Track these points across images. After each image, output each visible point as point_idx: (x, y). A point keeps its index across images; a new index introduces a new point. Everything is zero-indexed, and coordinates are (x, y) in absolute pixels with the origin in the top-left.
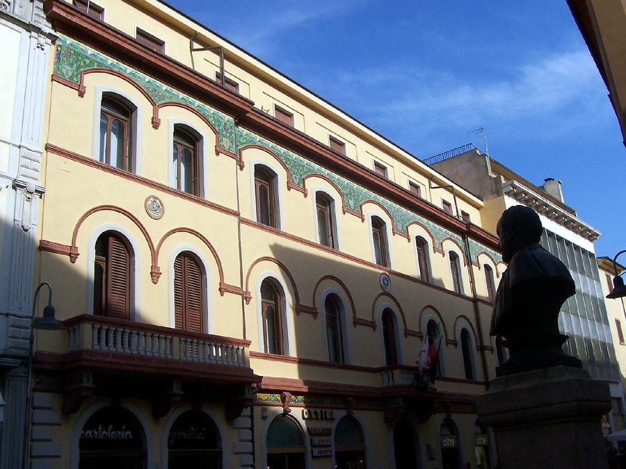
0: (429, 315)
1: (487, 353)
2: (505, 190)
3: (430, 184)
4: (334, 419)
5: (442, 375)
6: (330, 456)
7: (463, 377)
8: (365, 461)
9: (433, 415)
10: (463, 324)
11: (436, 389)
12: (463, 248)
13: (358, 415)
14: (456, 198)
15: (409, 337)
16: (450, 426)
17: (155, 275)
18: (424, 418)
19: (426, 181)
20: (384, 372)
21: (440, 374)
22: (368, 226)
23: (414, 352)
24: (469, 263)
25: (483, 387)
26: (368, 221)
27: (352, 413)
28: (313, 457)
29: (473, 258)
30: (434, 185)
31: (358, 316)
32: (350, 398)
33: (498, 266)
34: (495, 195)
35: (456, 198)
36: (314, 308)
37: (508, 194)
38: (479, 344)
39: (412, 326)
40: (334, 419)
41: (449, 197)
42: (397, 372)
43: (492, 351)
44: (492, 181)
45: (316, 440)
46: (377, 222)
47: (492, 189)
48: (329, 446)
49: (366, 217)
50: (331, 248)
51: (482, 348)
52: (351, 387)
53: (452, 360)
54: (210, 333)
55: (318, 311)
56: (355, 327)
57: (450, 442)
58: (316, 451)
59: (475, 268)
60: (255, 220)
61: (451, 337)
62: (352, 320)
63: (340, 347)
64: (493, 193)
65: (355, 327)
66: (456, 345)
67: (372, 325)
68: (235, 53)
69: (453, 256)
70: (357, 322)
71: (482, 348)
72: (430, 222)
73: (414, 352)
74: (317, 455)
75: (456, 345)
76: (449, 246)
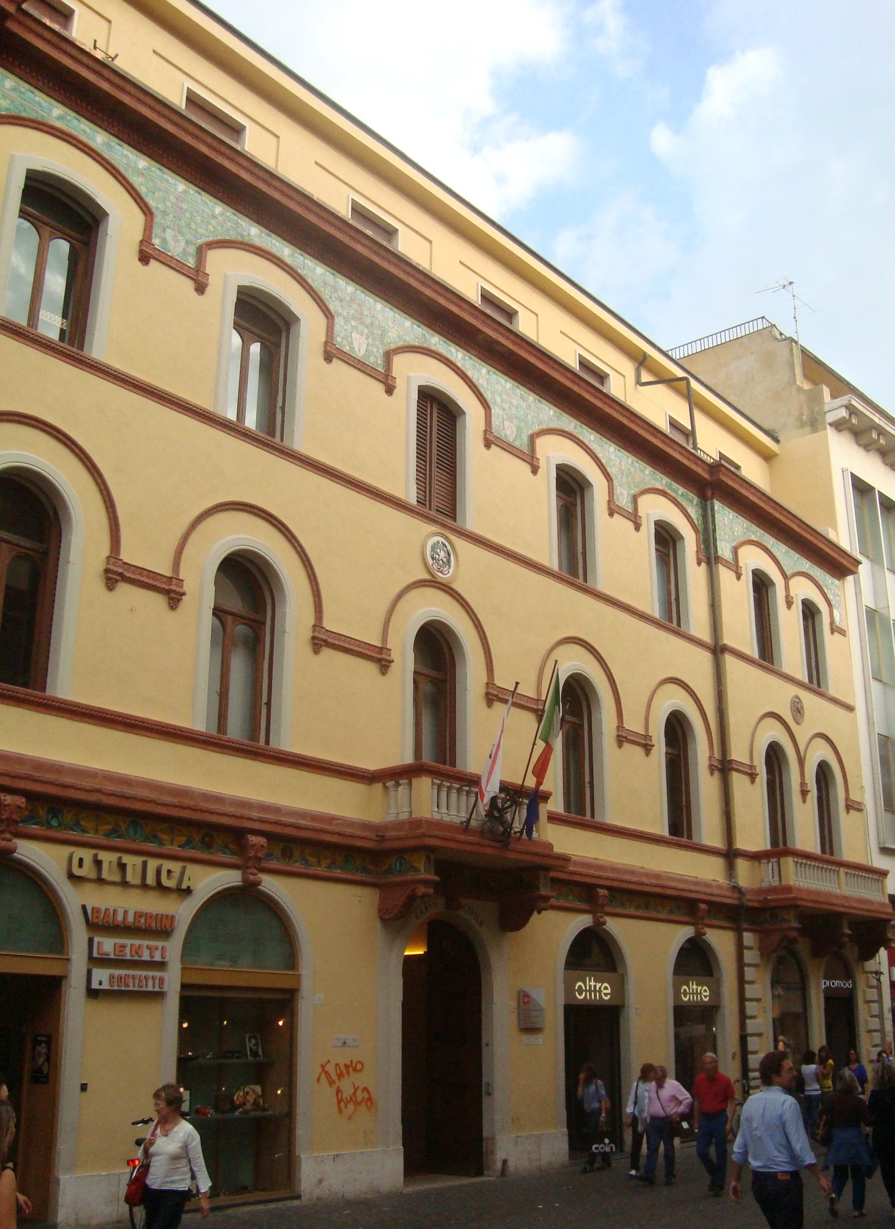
0: (573, 662)
1: (738, 781)
2: (831, 417)
3: (638, 376)
4: (188, 891)
5: (598, 818)
6: (158, 996)
7: (662, 829)
8: (180, 1024)
9: (536, 912)
10: (674, 700)
11: (550, 846)
12: (700, 528)
13: (614, 926)
14: (697, 413)
15: (626, 746)
16: (593, 952)
17: (804, 793)
18: (514, 917)
19: (627, 367)
20: (390, 784)
21: (267, 742)
22: (647, 538)
23: (501, 746)
24: (709, 556)
25: (718, 863)
26: (648, 531)
27: (604, 923)
28: (93, 994)
29: (724, 550)
30: (646, 377)
31: (126, 555)
32: (253, 839)
33: (793, 582)
34: (807, 429)
35: (697, 413)
36: (647, 737)
37: (838, 426)
38: (717, 755)
39: (349, 619)
40: (188, 891)
41: (680, 412)
42: (789, 863)
43: (752, 777)
44: (803, 397)
45: (108, 945)
46: (566, 477)
47: (802, 414)
48: (161, 965)
49: (644, 521)
50: (581, 581)
51: (724, 767)
52: (331, 819)
53: (632, 785)
54: (469, 771)
55: (654, 742)
56: (620, 746)
57: (595, 989)
58: (102, 977)
59: (725, 575)
60: (554, 566)
61: (634, 724)
62: (309, 634)
63: (587, 779)
64: (802, 425)
65: (620, 746)
66: (647, 748)
67: (381, 660)
68: (188, 14)
69: (666, 538)
70: (322, 641)
71: (724, 767)
72: (690, 494)
73: (501, 746)
74: (105, 986)
75: (647, 748)
76: (656, 509)
